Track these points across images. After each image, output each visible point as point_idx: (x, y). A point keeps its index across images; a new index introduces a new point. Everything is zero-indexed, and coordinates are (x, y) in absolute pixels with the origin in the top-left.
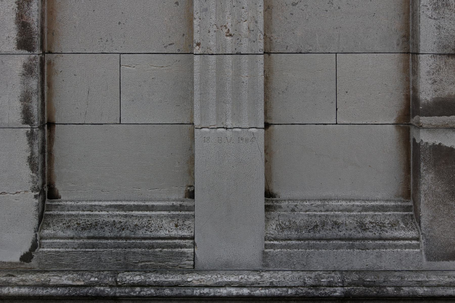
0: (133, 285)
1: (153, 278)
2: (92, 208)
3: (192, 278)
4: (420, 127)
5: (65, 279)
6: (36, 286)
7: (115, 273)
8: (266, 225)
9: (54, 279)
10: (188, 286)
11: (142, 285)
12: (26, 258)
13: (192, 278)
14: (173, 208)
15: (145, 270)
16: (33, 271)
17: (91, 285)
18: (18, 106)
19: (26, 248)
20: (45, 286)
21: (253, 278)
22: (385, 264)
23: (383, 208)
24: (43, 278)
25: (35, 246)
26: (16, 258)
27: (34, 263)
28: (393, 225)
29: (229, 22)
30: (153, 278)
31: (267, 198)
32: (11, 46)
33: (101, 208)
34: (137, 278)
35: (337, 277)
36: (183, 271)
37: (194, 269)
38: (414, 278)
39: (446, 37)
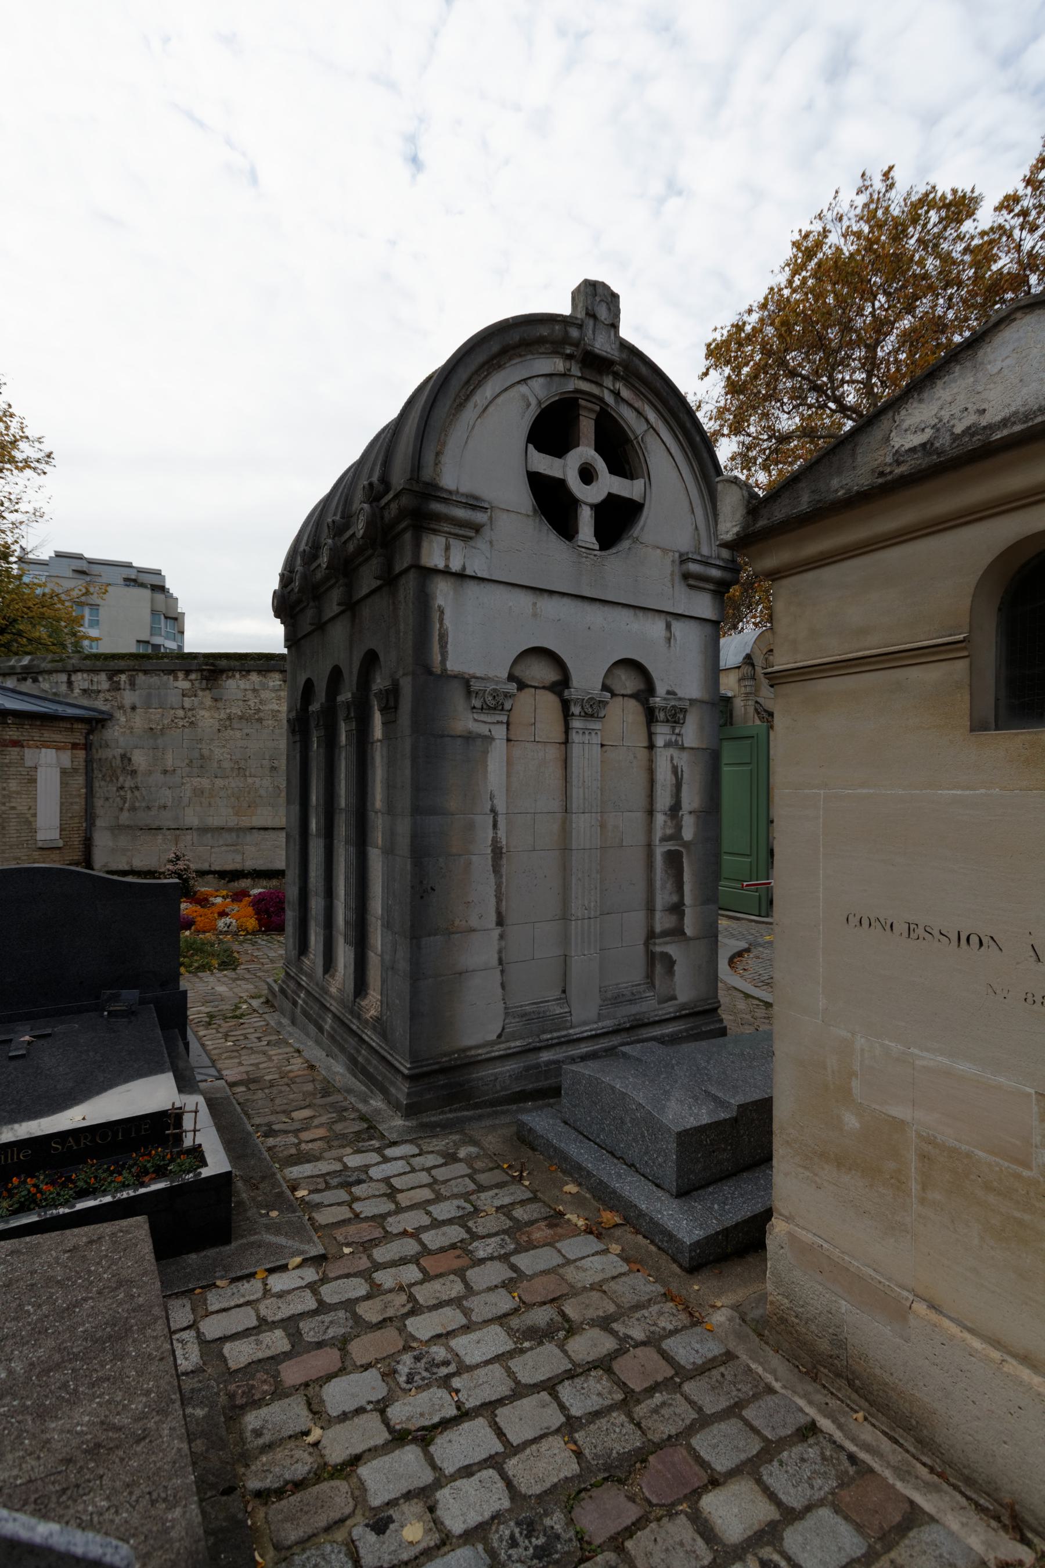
0: (548, 1040)
1: (555, 1035)
2: (521, 1006)
3: (571, 1031)
4: (655, 944)
5: (518, 1043)
6: (505, 1049)
7: (538, 1036)
8: (496, 1286)
9: (513, 1044)
10: (570, 1035)
11: (551, 1039)
12: (499, 1036)
13: (571, 1031)
14: (557, 999)
15: (551, 1032)
16: (503, 1043)
17: (529, 1044)
18: (496, 956)
19: (499, 1031)
20: (509, 1048)
21: (595, 1026)
22: (644, 1010)
23: (639, 985)
24: (508, 1044)
25: (503, 1029)
26: (495, 1037)
27: (503, 1038)
28: (644, 991)
29: (586, 903)
30: (555, 1035)
31: (718, 1026)
32: (493, 925)
33: (526, 1005)
34: (549, 1036)
35: (626, 1019)
36: (567, 1029)
37: (571, 1027)
38: (653, 1014)
39: (428, 1237)
